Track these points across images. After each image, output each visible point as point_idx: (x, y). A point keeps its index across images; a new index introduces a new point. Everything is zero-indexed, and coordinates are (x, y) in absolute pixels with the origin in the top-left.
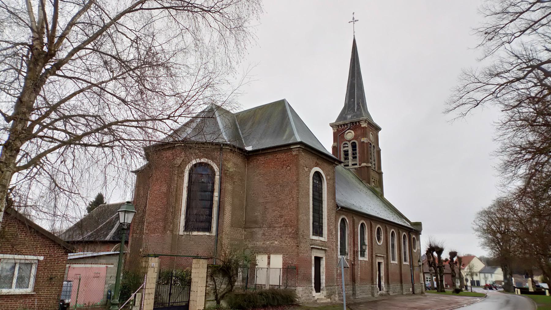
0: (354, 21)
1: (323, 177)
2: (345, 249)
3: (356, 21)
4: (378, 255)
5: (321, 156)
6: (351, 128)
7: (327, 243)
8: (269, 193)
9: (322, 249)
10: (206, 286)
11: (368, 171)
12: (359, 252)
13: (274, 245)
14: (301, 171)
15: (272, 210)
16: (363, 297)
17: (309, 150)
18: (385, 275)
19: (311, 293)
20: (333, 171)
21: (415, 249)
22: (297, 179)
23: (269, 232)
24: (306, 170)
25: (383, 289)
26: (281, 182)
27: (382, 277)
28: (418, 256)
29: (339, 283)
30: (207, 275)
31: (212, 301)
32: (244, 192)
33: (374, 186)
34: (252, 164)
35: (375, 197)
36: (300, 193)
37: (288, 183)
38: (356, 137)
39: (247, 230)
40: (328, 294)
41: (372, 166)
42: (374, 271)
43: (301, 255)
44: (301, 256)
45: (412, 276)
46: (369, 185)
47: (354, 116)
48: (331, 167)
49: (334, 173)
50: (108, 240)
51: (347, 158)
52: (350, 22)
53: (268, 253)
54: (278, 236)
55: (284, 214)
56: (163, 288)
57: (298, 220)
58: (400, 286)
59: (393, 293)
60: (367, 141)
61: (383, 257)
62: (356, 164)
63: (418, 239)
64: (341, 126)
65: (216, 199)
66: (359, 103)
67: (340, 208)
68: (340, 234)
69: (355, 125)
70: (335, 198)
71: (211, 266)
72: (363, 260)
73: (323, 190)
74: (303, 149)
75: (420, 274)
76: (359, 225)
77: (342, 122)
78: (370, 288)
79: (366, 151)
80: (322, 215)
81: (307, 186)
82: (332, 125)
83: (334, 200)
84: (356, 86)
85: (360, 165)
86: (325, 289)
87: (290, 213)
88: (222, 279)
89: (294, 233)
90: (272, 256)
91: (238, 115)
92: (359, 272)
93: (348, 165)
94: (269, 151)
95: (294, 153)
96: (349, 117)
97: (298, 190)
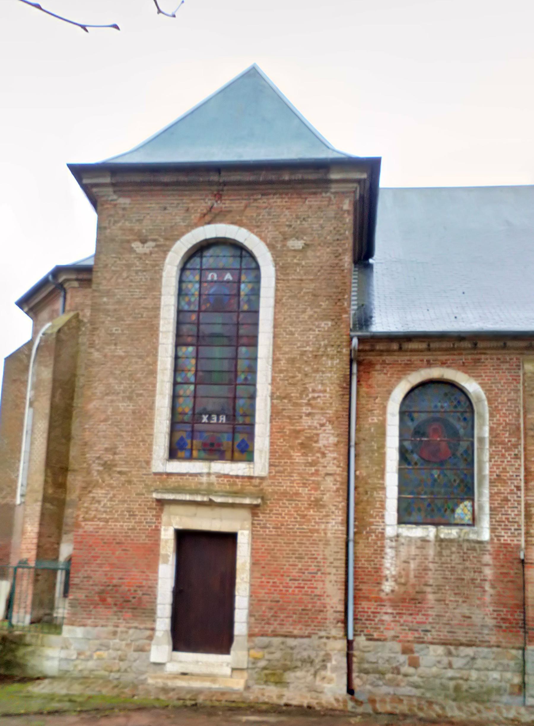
19: (141, 649)
36: (102, 332)
81: (147, 302)
86: (246, 645)
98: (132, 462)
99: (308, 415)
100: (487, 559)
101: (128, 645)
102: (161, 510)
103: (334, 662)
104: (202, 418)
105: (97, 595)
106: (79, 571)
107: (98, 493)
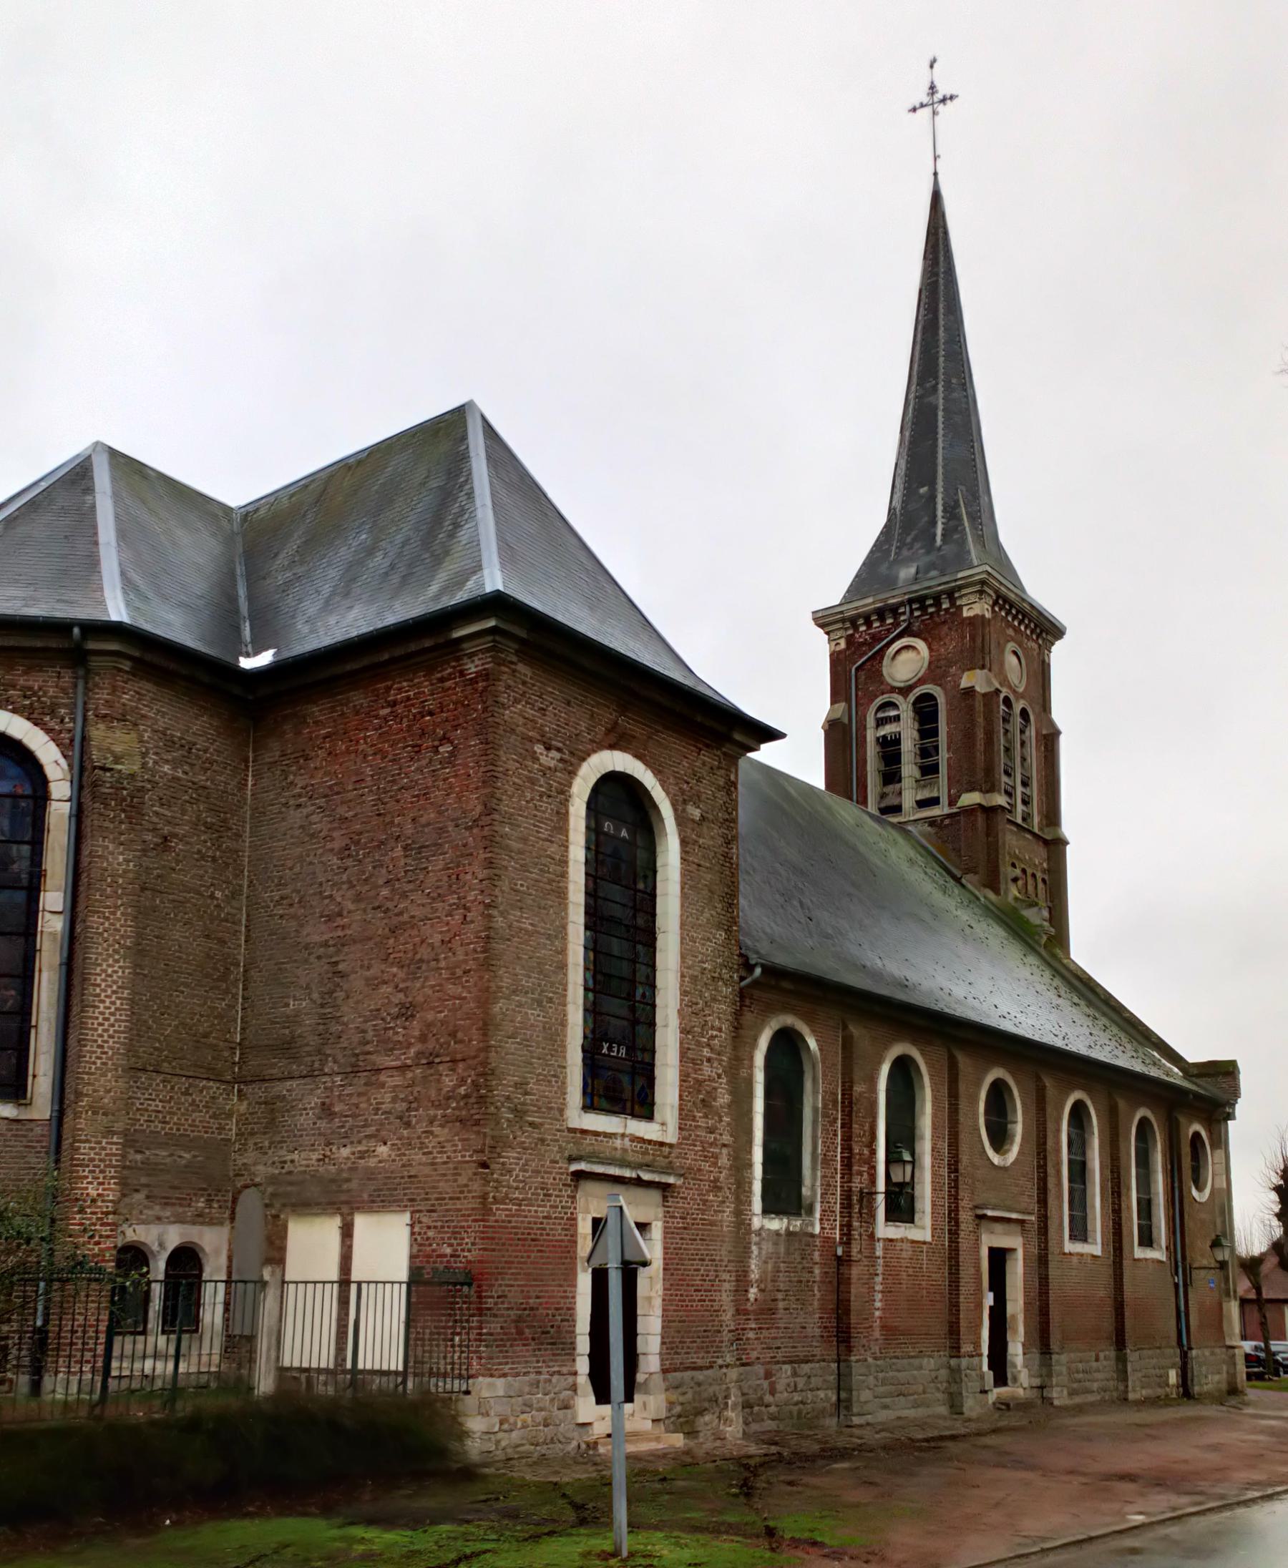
0: (936, 99)
3: (943, 100)
4: (990, 1213)
6: (915, 627)
7: (676, 1151)
8: (350, 893)
9: (639, 1182)
11: (990, 831)
12: (881, 1200)
13: (372, 1162)
14: (508, 760)
15: (367, 979)
16: (899, 1418)
18: (1026, 1310)
21: (1200, 1189)
23: (350, 1095)
24: (549, 759)
25: (1015, 1379)
26: (409, 829)
27: (1013, 1316)
28: (1219, 1221)
29: (754, 1354)
33: (1016, 899)
35: (1014, 951)
37: (442, 830)
38: (935, 672)
40: (678, 1409)
41: (1013, 806)
42: (966, 1288)
44: (501, 1215)
45: (1182, 1315)
46: (992, 896)
47: (932, 566)
48: (708, 758)
49: (729, 794)
51: (891, 776)
52: (914, 110)
53: (345, 1209)
55: (420, 999)
56: (442, 1367)
57: (486, 1026)
58: (1113, 1362)
59: (1072, 1393)
60: (989, 683)
61: (1022, 1222)
62: (934, 801)
63: (1220, 1141)
64: (869, 623)
65: (52, 924)
66: (957, 502)
67: (758, 971)
69: (931, 610)
72: (902, 1240)
75: (1225, 1305)
77: (870, 600)
78: (943, 1373)
79: (980, 734)
80: (654, 1006)
81: (553, 849)
82: (824, 620)
84: (940, 419)
85: (952, 803)
86: (663, 1386)
87: (451, 989)
89: (466, 1096)
90: (362, 1223)
91: (250, 513)
92: (879, 1296)
93: (897, 809)
94: (349, 667)
95: (472, 668)
96: (907, 572)
97: (490, 864)
98: (544, 1110)
101: (552, 1400)
103: (733, 1398)
105: (513, 1325)
107: (510, 1156)
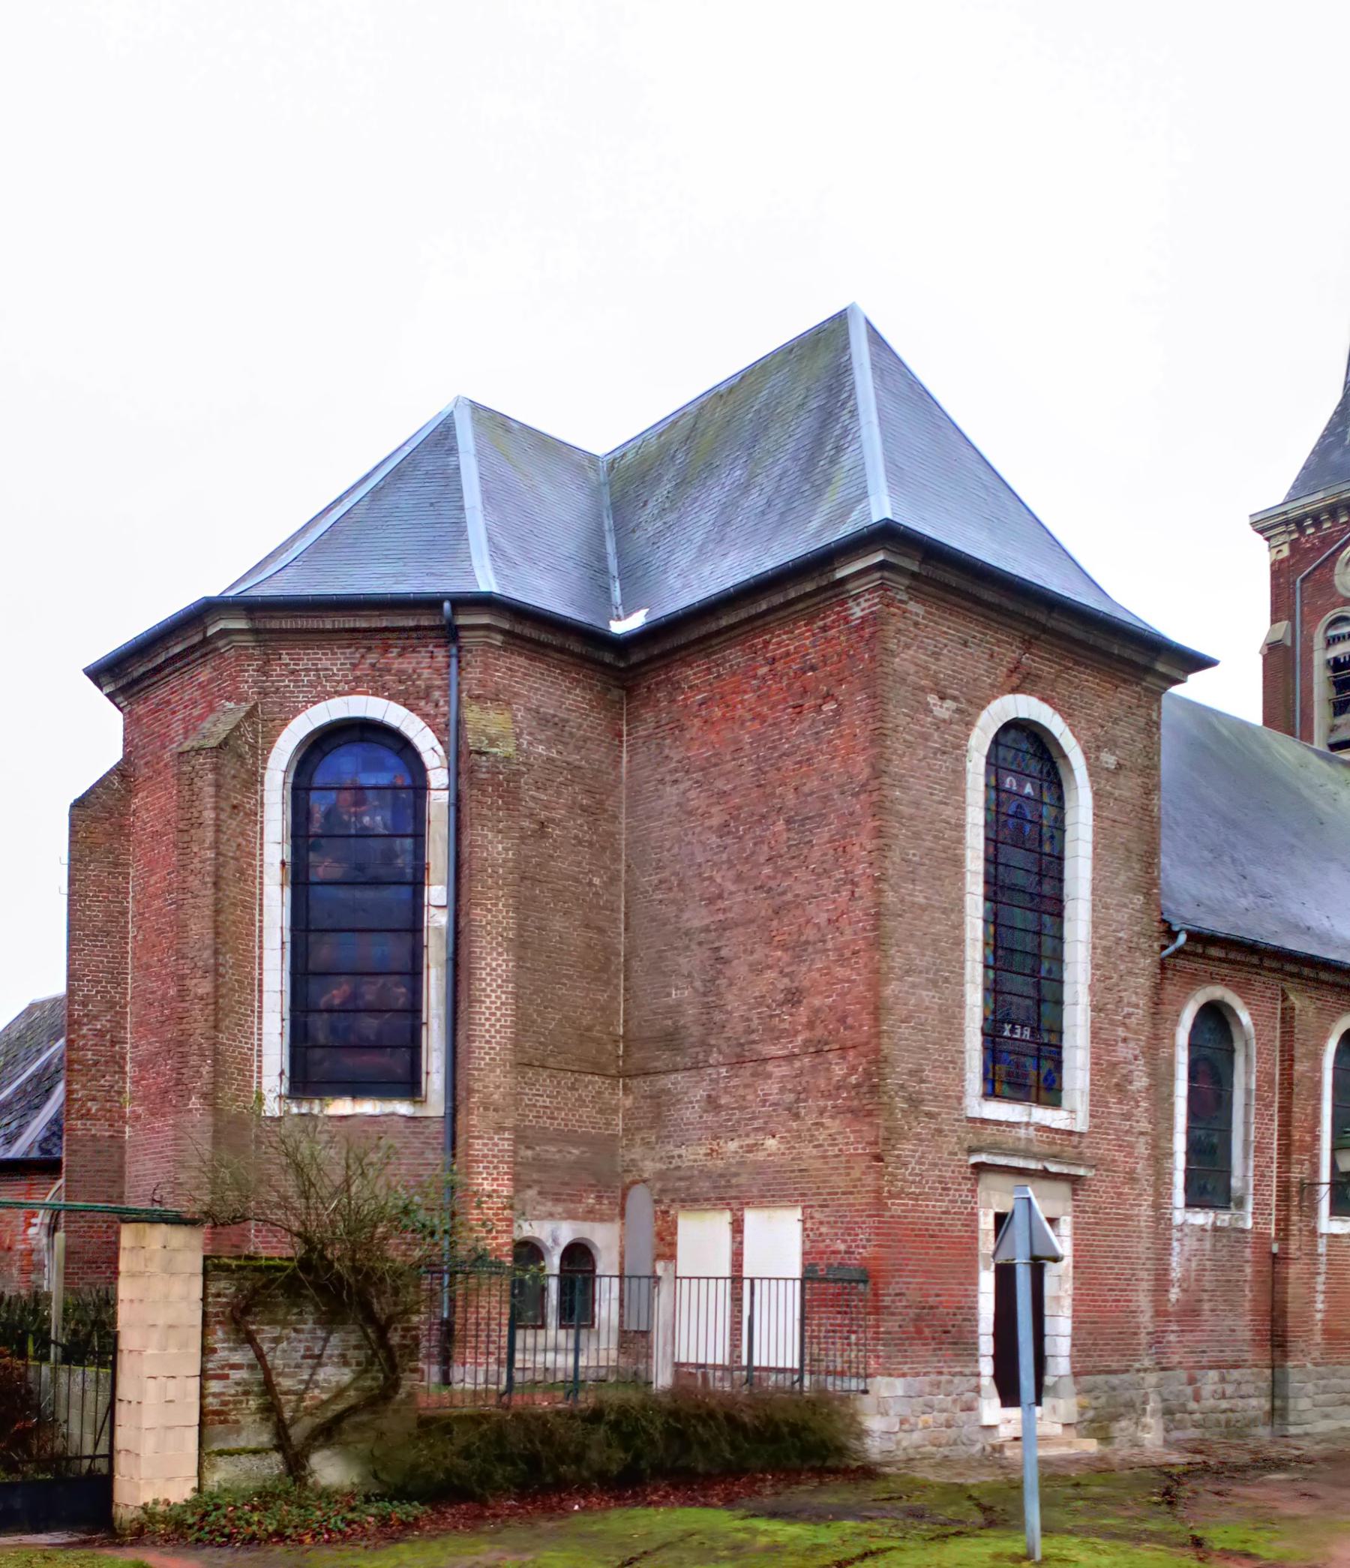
1: (1065, 757)
2: (1227, 1173)
5: (1052, 623)
7: (1086, 1141)
9: (1045, 1175)
10: (204, 1375)
12: (1324, 1191)
13: (761, 1156)
14: (898, 715)
15: (751, 965)
17: (952, 579)
19: (969, 1408)
20: (1142, 722)
22: (873, 767)
24: (944, 710)
26: (791, 799)
30: (205, 1314)
31: (255, 1452)
32: (613, 879)
34: (648, 715)
36: (895, 856)
37: (826, 799)
39: (633, 1083)
40: (1090, 1414)
43: (896, 1207)
44: (896, 1210)
48: (1126, 695)
50: (19, 1156)
53: (735, 1204)
54: (780, 1111)
55: (806, 983)
57: (877, 1010)
64: (1317, 523)
65: (437, 920)
67: (1182, 938)
68: (1192, 1091)
70: (1154, 883)
71: (234, 1263)
73: (1068, 836)
74: (914, 575)
76: (1325, 1038)
77: (1320, 495)
80: (1061, 982)
81: (948, 812)
82: (1264, 526)
83: (1147, 894)
86: (1074, 1389)
87: (840, 972)
88: (320, 1333)
89: (858, 1086)
92: (1320, 1297)
95: (857, 612)
97: (879, 833)
99: (1125, 1040)
100: (1248, 1253)
101: (954, 1401)
102: (977, 1181)
104: (1003, 1030)
106: (890, 1283)
107: (906, 1148)
